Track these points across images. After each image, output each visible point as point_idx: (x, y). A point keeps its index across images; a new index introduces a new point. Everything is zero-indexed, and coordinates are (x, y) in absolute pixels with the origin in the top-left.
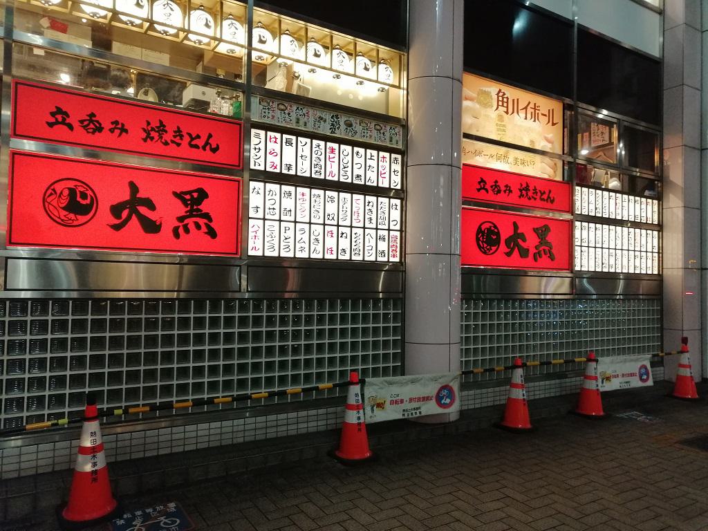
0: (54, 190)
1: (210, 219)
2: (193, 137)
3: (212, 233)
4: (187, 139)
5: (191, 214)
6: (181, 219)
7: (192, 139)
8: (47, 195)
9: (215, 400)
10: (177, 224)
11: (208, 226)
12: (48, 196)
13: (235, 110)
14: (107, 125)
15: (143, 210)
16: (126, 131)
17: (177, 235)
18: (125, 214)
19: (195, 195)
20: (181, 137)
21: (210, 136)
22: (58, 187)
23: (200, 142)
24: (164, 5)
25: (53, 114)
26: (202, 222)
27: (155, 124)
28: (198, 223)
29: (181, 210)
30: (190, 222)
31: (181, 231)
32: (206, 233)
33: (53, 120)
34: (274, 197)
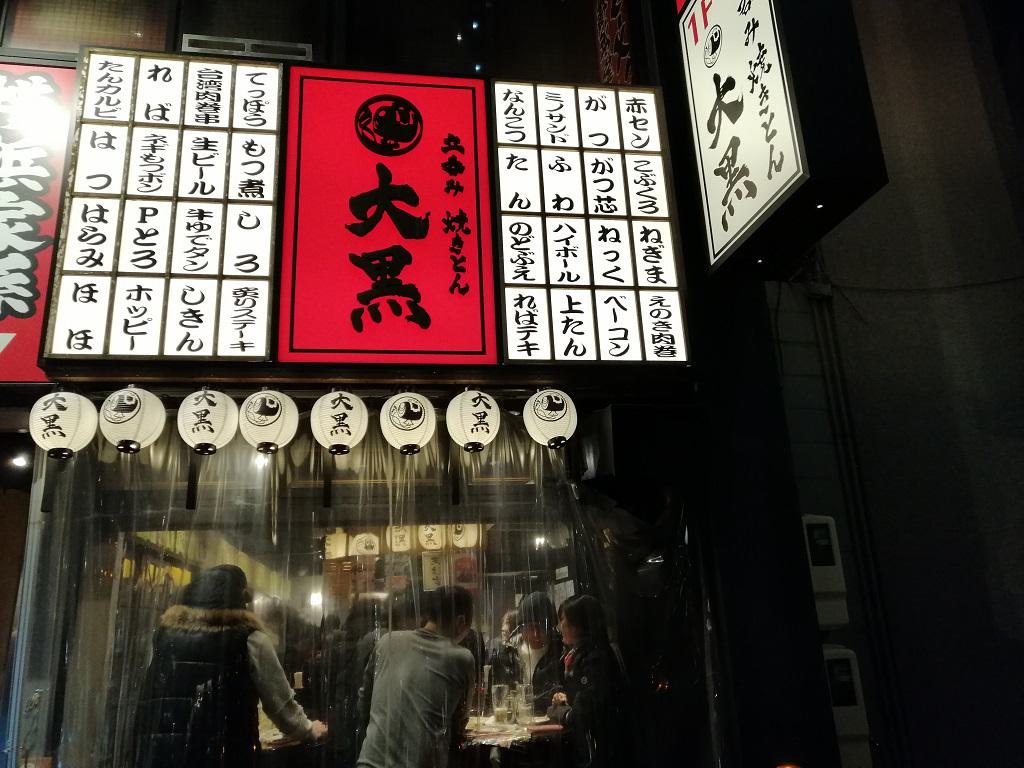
3: (421, 319)
5: (379, 290)
9: (124, 576)
10: (358, 305)
11: (413, 306)
13: (532, 697)
15: (399, 205)
17: (358, 326)
24: (474, 400)
28: (395, 301)
30: (339, 429)
31: (366, 317)
32: (409, 318)
34: (607, 175)
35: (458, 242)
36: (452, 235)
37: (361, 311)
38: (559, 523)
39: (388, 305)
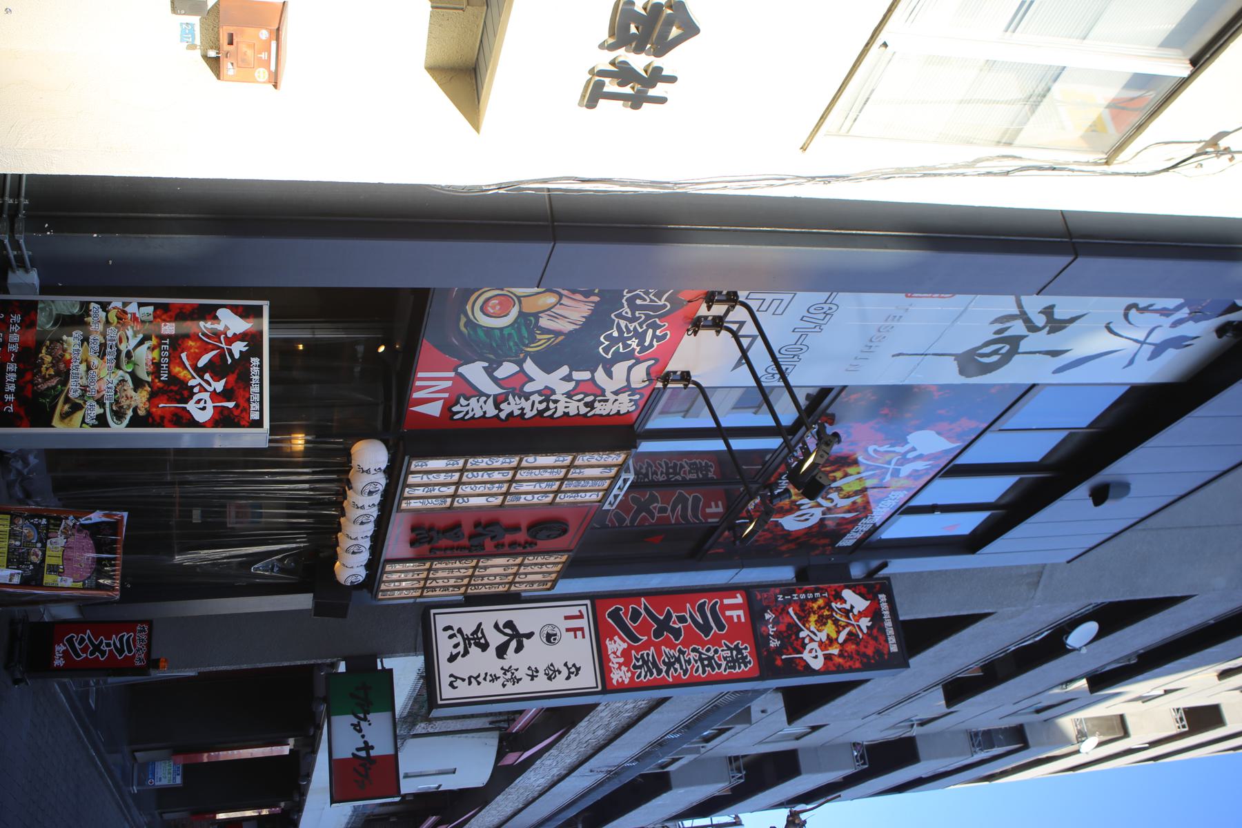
1: (463, 656)
3: (452, 658)
6: (460, 631)
15: (514, 644)
17: (446, 629)
18: (508, 631)
19: (482, 641)
26: (461, 649)
29: (468, 631)
30: (459, 639)
31: (450, 632)
35: (495, 678)
36: (500, 673)
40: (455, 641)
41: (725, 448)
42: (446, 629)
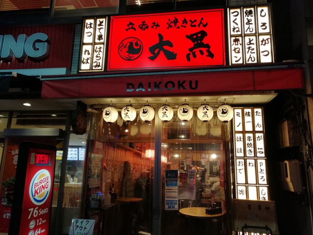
0: (123, 44)
2: (193, 21)
3: (211, 55)
4: (189, 23)
6: (191, 50)
7: (192, 22)
8: (120, 46)
10: (189, 52)
11: (208, 51)
12: (120, 48)
14: (150, 25)
16: (159, 26)
17: (189, 60)
20: (186, 23)
21: (202, 19)
22: (125, 43)
23: (196, 23)
25: (128, 25)
27: (173, 19)
29: (163, 114)
30: (205, 116)
31: (191, 56)
32: (207, 56)
33: (128, 28)
37: (190, 54)
38: (214, 190)
39: (199, 52)
40: (205, 116)
41: (308, 139)
42: (189, 60)
